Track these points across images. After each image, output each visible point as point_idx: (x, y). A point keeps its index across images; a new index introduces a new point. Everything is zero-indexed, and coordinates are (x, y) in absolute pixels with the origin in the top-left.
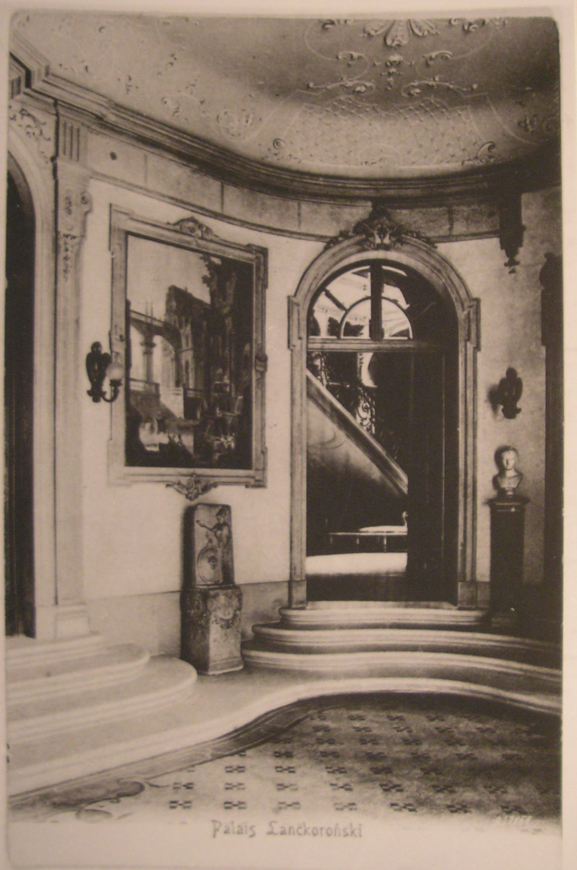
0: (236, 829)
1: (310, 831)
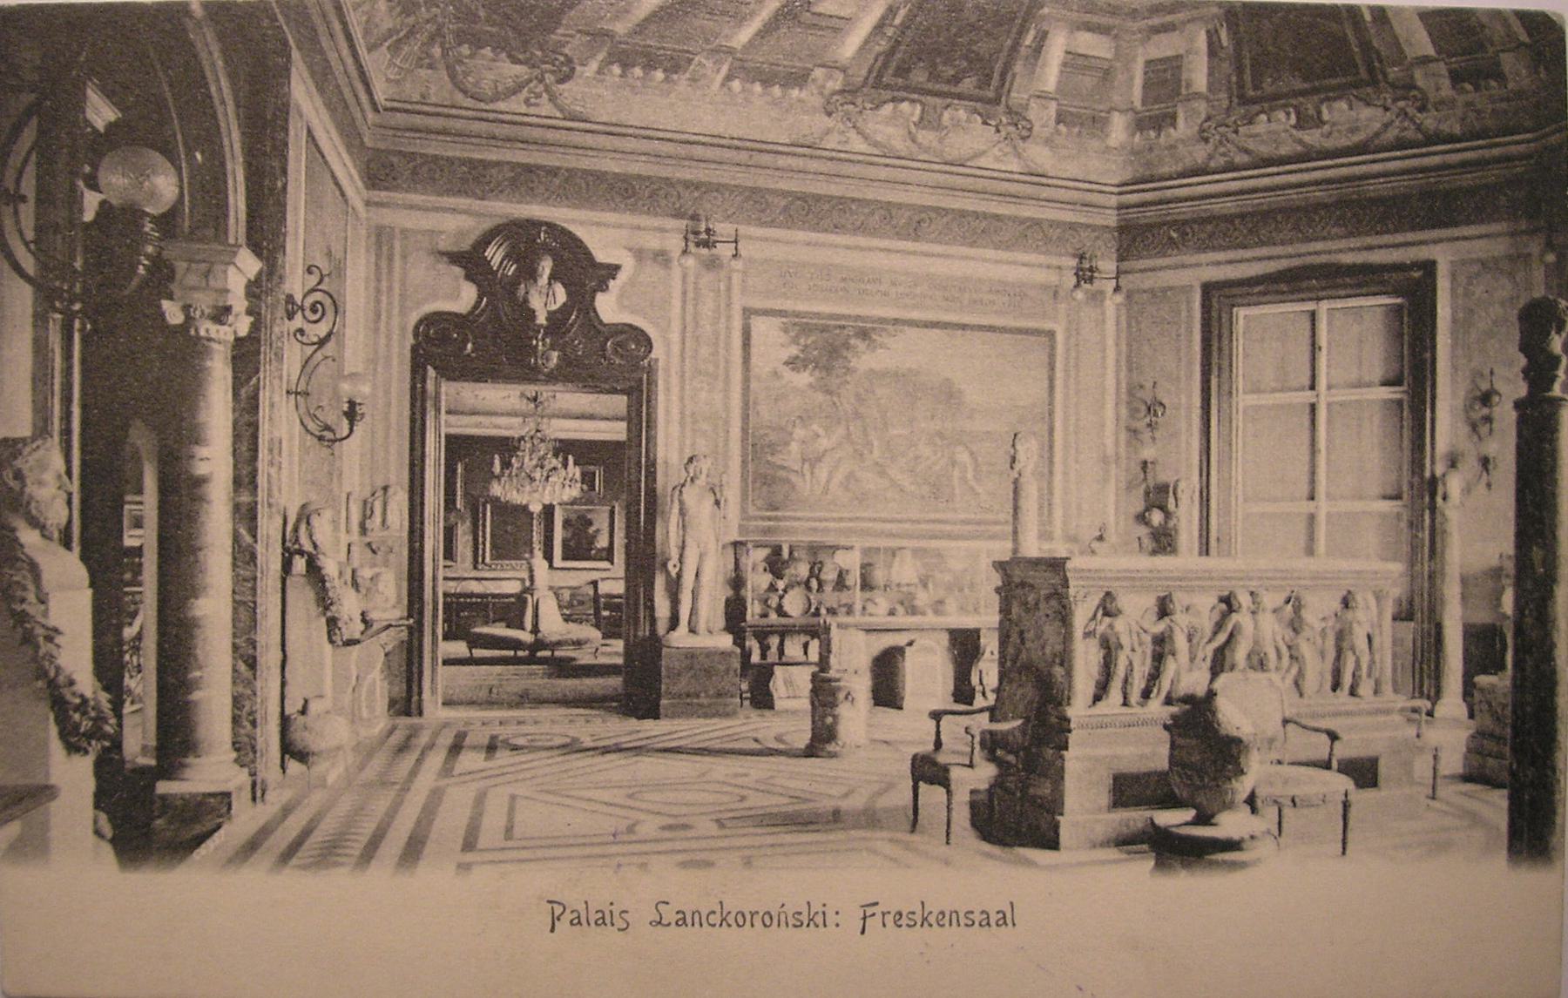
1: (731, 919)
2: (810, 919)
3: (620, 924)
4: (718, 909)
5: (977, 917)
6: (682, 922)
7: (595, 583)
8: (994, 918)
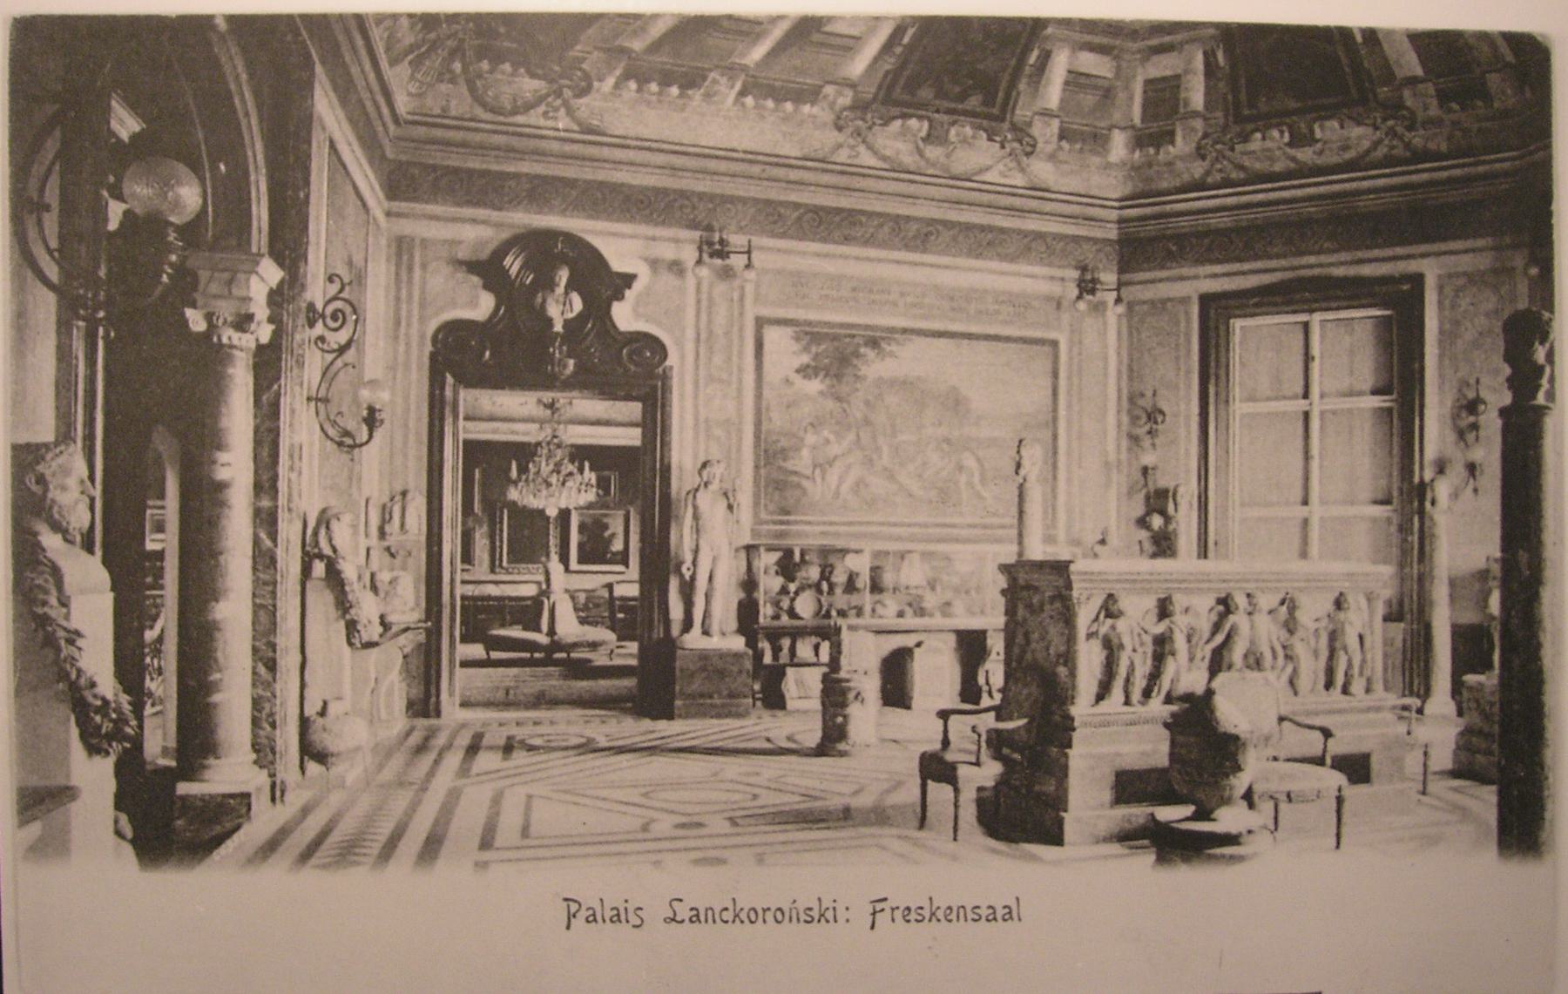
0: (609, 914)
1: (743, 916)
2: (819, 915)
3: (635, 920)
4: (731, 907)
5: (984, 912)
6: (695, 918)
7: (610, 587)
8: (1000, 912)
